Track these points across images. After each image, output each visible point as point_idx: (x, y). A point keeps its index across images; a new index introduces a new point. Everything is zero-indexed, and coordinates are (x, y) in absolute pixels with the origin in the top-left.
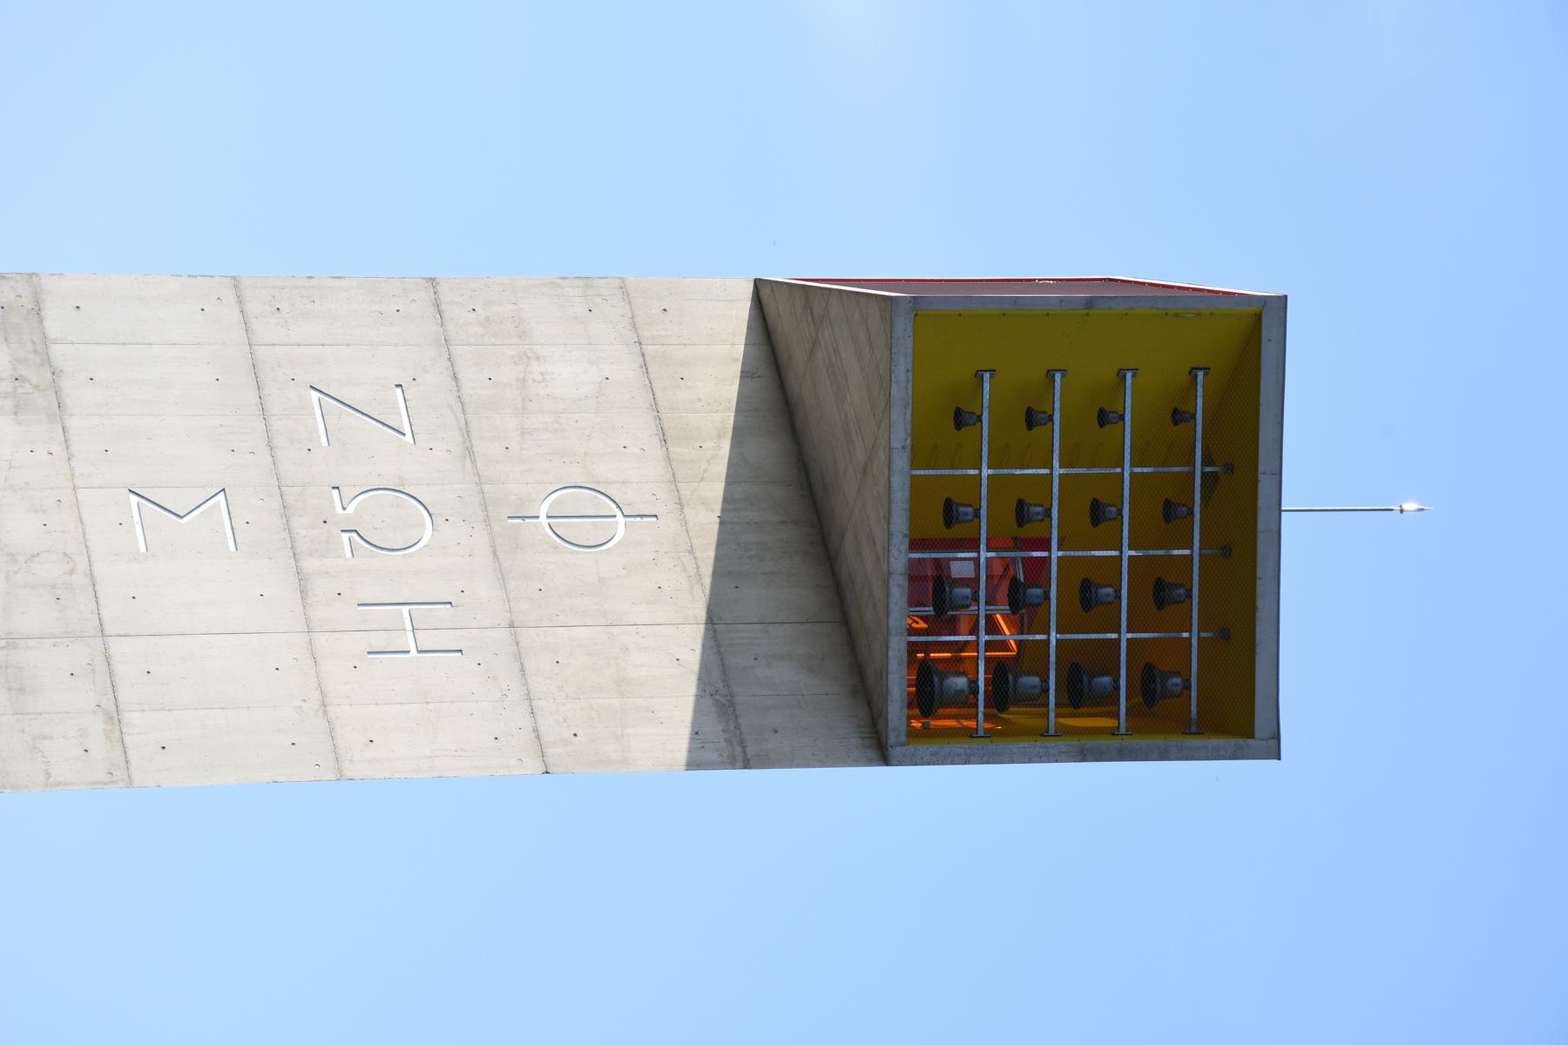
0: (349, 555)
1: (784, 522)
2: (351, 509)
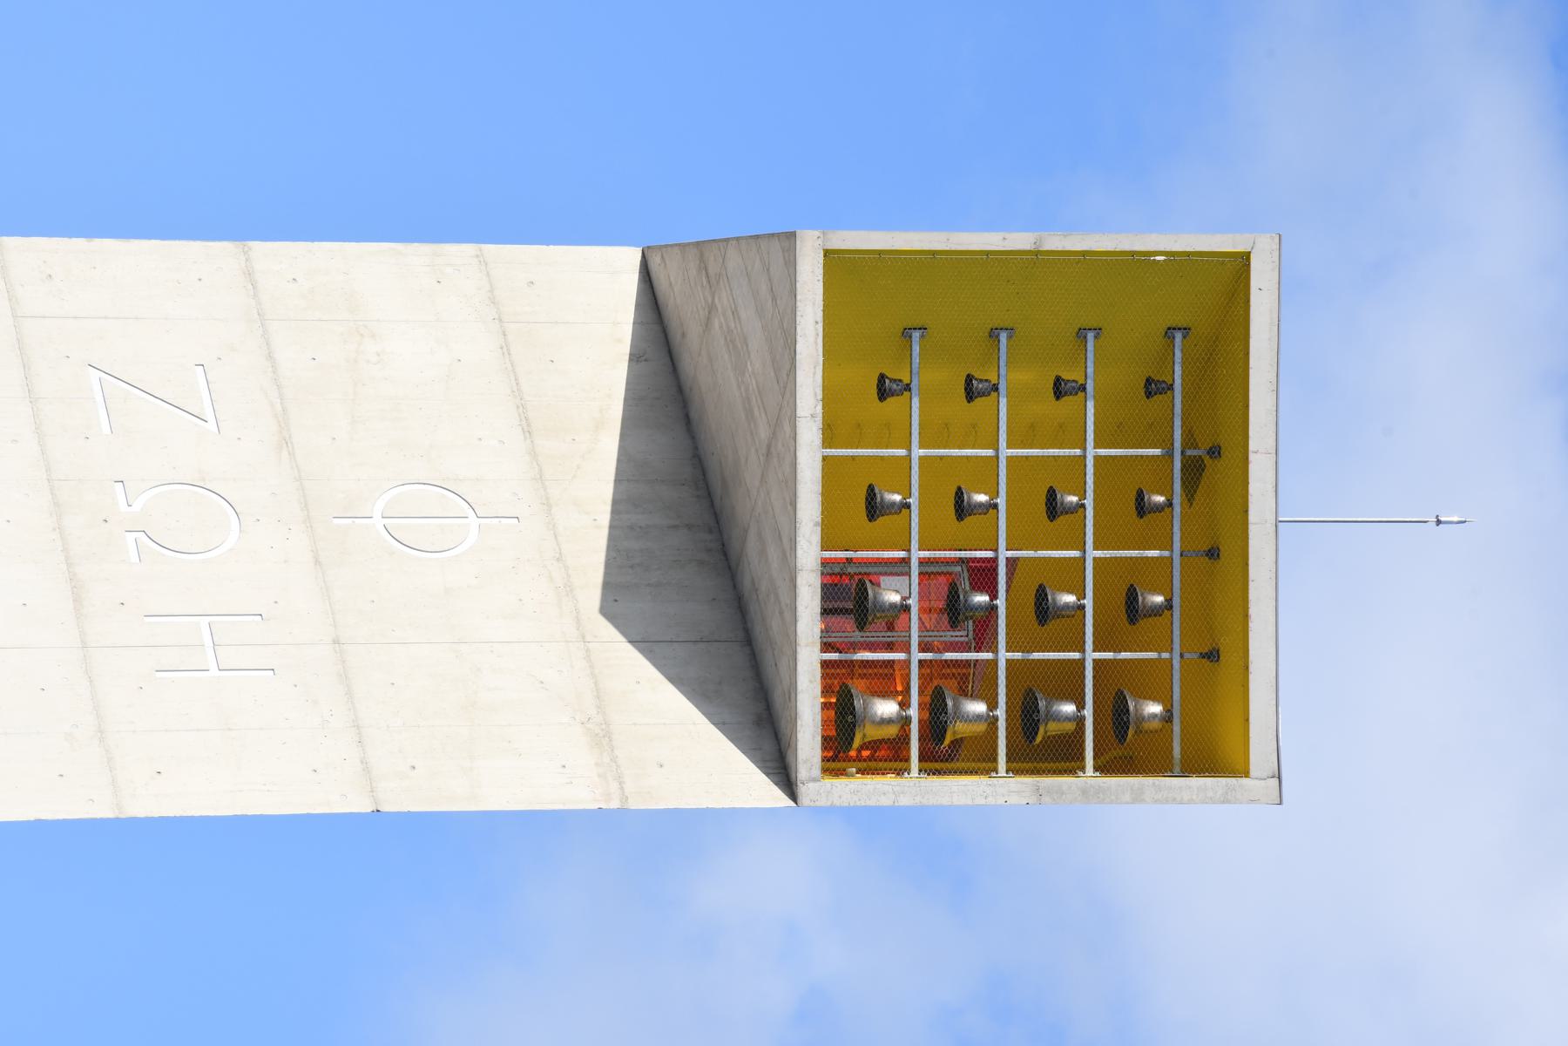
0: (134, 558)
1: (675, 527)
2: (137, 506)
